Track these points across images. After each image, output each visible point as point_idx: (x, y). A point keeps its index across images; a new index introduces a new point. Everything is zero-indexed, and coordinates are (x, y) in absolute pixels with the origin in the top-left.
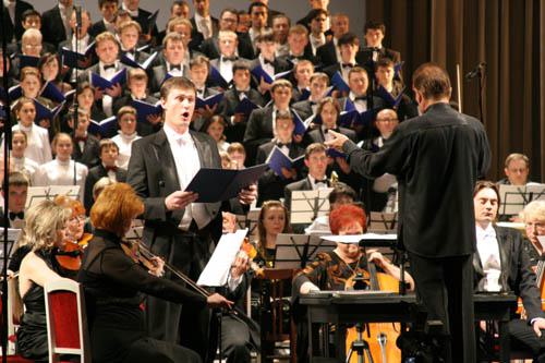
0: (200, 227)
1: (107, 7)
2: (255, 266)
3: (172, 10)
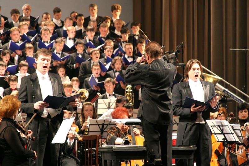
0: (52, 117)
1: (14, 16)
2: (78, 136)
3: (42, 17)
